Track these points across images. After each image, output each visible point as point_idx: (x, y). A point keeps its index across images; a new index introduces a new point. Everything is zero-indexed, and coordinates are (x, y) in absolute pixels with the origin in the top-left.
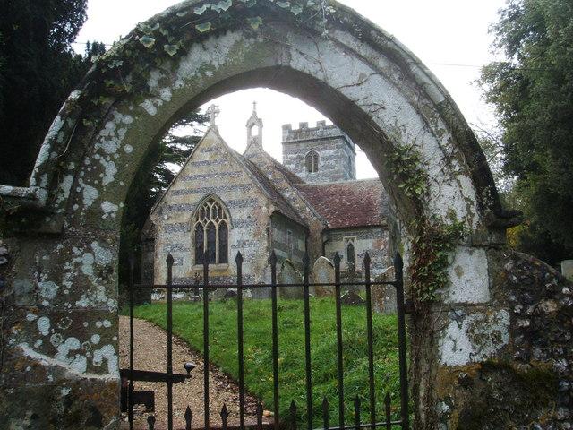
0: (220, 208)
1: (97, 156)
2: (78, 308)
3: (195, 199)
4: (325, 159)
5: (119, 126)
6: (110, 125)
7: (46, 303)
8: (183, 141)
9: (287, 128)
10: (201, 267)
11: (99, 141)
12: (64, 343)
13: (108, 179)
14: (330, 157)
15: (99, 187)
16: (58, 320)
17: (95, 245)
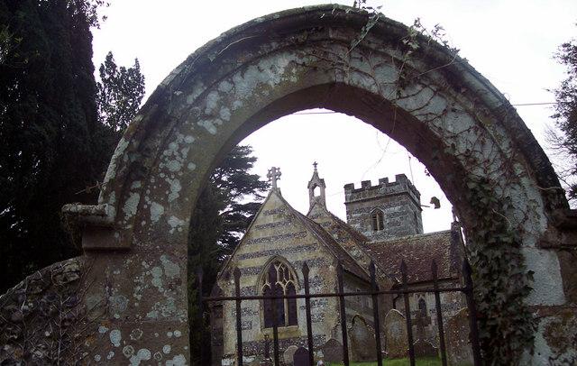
0: (287, 269)
1: (162, 175)
2: (149, 319)
3: (260, 262)
4: (389, 216)
5: (181, 146)
6: (174, 146)
7: (117, 316)
8: (246, 208)
9: (349, 187)
10: (270, 331)
11: (164, 162)
12: (135, 354)
13: (174, 195)
14: (395, 214)
15: (165, 204)
16: (130, 333)
17: (164, 259)
